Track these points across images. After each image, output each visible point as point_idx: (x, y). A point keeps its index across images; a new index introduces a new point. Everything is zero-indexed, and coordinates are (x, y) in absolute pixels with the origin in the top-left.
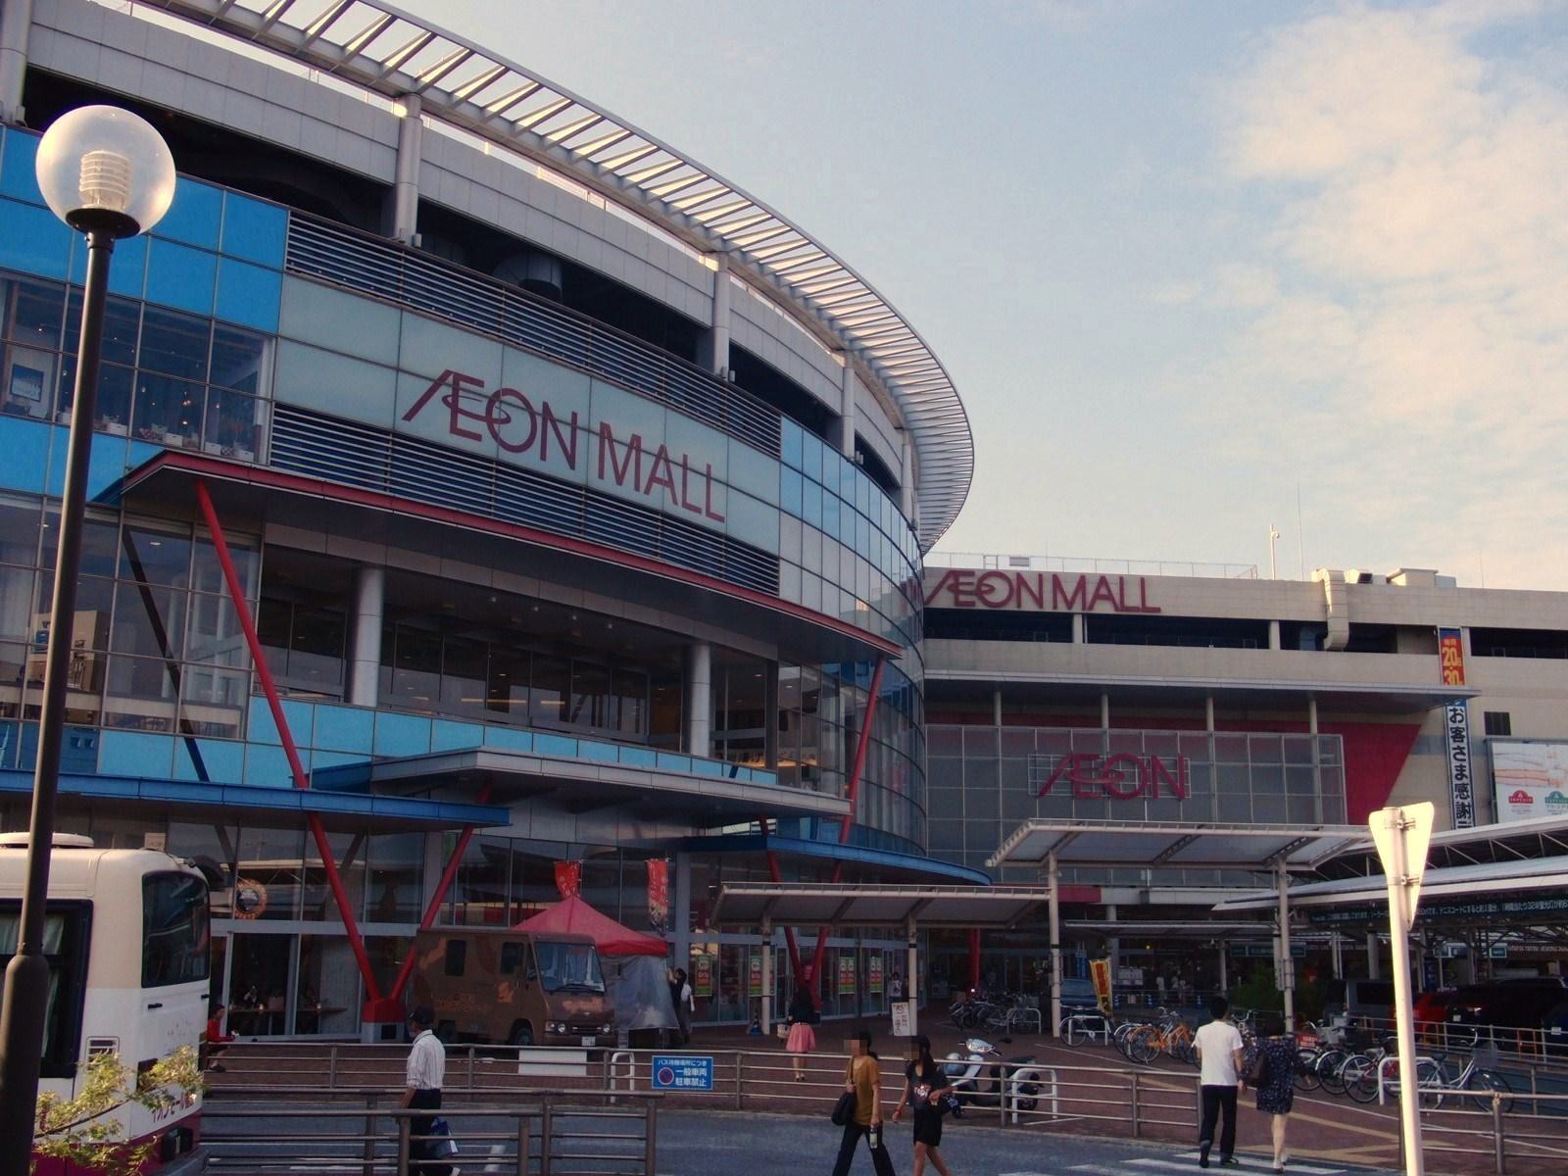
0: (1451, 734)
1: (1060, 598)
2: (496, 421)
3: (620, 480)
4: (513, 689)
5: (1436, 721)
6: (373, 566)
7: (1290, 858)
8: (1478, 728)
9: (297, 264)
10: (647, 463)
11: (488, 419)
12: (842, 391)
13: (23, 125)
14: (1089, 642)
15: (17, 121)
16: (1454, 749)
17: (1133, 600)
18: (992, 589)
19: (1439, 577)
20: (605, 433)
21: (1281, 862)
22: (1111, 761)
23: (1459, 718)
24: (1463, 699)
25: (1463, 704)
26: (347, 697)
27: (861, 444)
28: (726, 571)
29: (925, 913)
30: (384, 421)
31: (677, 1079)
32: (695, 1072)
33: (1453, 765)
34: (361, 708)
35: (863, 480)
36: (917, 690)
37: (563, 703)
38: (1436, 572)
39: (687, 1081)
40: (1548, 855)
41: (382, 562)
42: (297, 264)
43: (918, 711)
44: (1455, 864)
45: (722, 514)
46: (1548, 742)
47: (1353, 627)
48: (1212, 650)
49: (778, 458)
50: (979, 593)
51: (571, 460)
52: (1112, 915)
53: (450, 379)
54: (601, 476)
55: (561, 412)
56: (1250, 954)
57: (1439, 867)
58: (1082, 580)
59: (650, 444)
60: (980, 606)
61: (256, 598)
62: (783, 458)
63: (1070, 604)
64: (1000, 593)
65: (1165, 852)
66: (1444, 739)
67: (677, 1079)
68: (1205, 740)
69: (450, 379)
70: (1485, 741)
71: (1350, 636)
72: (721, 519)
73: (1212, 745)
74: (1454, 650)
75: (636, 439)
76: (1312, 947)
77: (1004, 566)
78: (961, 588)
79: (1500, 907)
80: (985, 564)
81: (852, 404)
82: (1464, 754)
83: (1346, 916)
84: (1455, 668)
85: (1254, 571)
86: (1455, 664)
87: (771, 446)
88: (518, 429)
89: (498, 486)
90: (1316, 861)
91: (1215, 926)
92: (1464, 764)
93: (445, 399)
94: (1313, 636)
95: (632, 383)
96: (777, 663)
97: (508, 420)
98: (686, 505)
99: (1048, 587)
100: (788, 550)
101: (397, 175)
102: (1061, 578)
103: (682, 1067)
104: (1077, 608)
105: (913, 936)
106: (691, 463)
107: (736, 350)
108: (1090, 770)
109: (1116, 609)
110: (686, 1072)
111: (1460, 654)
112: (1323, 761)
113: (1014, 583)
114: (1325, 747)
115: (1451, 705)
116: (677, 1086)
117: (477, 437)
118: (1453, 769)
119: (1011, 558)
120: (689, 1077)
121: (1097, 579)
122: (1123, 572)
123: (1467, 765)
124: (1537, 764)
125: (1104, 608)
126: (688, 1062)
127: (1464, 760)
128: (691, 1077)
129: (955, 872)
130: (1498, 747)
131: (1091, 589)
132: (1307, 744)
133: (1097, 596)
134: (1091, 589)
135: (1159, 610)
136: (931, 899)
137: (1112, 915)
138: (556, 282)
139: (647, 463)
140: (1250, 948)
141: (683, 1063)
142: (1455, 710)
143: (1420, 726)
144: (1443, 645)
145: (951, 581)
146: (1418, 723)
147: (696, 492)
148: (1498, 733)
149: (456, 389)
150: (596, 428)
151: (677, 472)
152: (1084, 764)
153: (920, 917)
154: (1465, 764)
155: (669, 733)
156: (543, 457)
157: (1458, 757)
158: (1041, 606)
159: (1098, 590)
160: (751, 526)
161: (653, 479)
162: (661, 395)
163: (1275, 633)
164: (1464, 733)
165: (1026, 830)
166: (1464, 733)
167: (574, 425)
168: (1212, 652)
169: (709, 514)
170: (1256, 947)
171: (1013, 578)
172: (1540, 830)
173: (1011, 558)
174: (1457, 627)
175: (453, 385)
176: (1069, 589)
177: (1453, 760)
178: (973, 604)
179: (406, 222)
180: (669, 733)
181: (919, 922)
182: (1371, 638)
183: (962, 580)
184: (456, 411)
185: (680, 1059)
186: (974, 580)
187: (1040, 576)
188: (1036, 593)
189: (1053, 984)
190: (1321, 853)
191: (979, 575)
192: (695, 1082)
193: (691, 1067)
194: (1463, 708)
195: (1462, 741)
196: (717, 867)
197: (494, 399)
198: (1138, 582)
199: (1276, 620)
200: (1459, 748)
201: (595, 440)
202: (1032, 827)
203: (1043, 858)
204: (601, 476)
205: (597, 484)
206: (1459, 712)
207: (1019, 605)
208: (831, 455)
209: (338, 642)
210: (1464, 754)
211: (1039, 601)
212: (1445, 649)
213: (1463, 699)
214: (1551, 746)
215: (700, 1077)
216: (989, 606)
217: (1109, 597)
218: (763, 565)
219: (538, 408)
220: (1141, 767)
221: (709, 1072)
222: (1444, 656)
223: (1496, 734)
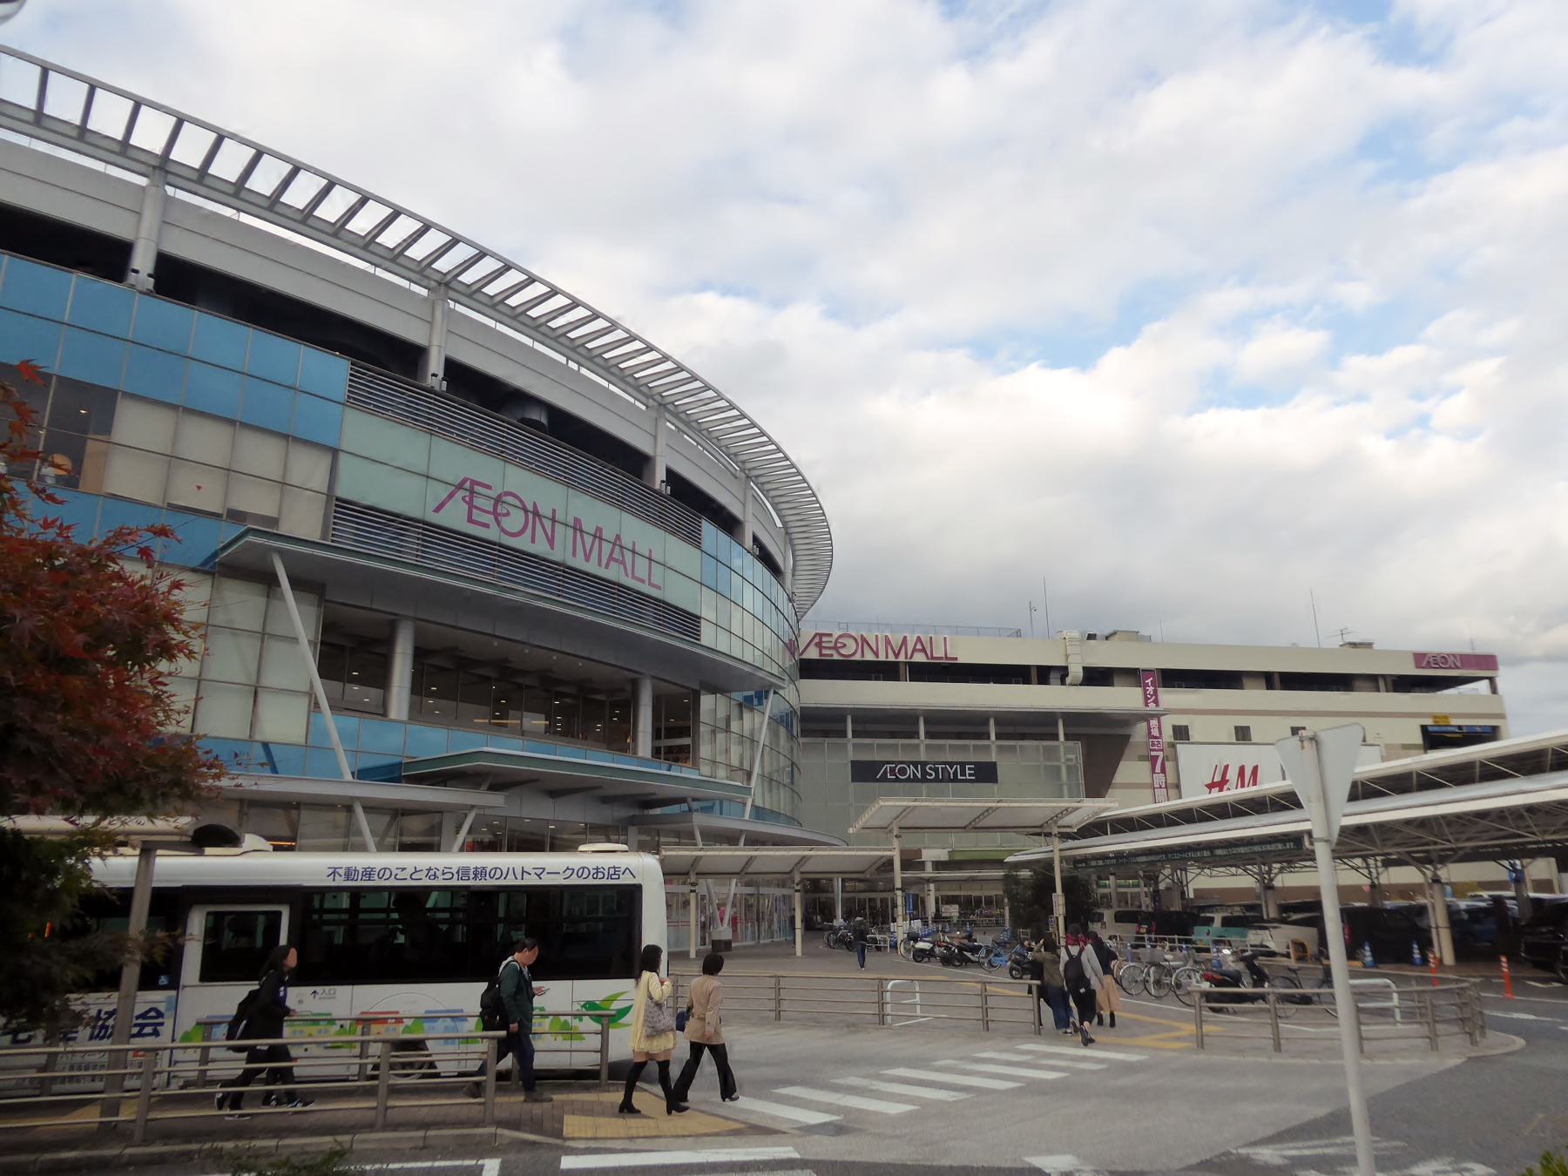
2: (500, 514)
3: (587, 558)
4: (511, 712)
6: (406, 618)
7: (1061, 823)
9: (354, 399)
10: (607, 548)
11: (496, 515)
12: (744, 505)
13: (152, 292)
15: (148, 290)
19: (1141, 636)
20: (577, 527)
21: (1053, 825)
23: (600, 875)
24: (1158, 716)
26: (384, 714)
27: (756, 540)
28: (663, 621)
29: (807, 867)
30: (415, 512)
34: (395, 721)
35: (759, 566)
36: (796, 713)
37: (548, 722)
40: (1234, 816)
41: (412, 614)
42: (354, 399)
43: (796, 728)
44: (1235, 815)
48: (992, 685)
49: (699, 547)
50: (835, 648)
51: (551, 541)
52: (929, 867)
53: (467, 485)
54: (574, 554)
55: (545, 510)
57: (1131, 831)
59: (609, 534)
60: (836, 657)
61: (318, 639)
63: (897, 656)
65: (974, 820)
69: (467, 485)
72: (659, 588)
75: (599, 530)
78: (824, 645)
79: (1212, 852)
81: (751, 515)
83: (1101, 863)
87: (694, 539)
88: (515, 521)
89: (500, 556)
90: (1076, 825)
93: (463, 498)
94: (1059, 676)
95: (598, 493)
97: (508, 514)
98: (634, 577)
100: (707, 612)
101: (430, 341)
106: (637, 549)
107: (670, 472)
109: (928, 658)
114: (1068, 750)
117: (486, 526)
125: (919, 658)
129: (816, 837)
133: (915, 650)
135: (956, 659)
136: (811, 856)
137: (929, 867)
138: (544, 420)
139: (607, 548)
145: (817, 640)
149: (472, 492)
150: (571, 522)
151: (628, 556)
153: (802, 869)
155: (620, 739)
156: (533, 541)
158: (877, 656)
159: (915, 645)
160: (679, 594)
161: (611, 558)
162: (620, 503)
163: (1034, 674)
165: (877, 806)
167: (554, 520)
169: (650, 584)
172: (1194, 805)
175: (468, 488)
178: (832, 655)
179: (435, 365)
180: (620, 739)
181: (802, 873)
182: (1097, 677)
183: (824, 639)
184: (471, 506)
190: (1080, 819)
196: (657, 839)
197: (498, 500)
201: (570, 532)
202: (882, 803)
203: (889, 825)
204: (574, 554)
205: (571, 562)
207: (863, 655)
208: (736, 548)
209: (379, 677)
211: (876, 654)
213: (1158, 716)
217: (924, 650)
218: (689, 622)
219: (530, 507)
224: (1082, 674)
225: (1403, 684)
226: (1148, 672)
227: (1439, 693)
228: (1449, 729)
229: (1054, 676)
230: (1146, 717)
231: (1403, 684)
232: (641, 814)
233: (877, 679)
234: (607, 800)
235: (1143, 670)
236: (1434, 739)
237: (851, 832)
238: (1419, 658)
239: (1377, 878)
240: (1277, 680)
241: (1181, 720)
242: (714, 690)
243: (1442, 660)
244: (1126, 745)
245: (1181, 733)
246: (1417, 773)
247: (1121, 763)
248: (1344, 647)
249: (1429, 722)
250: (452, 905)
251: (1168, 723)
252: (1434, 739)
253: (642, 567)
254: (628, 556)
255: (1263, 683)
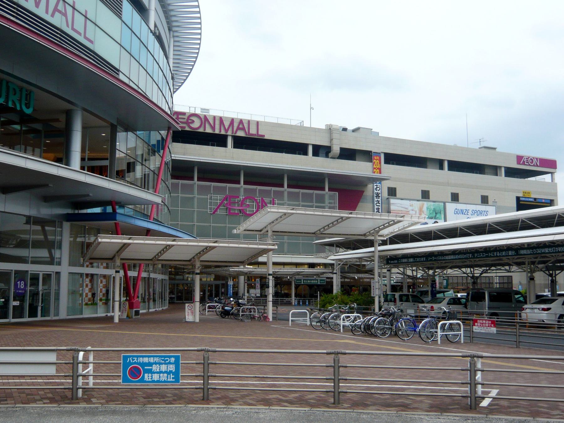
0: (375, 195)
1: (222, 128)
5: (370, 189)
8: (385, 194)
14: (234, 148)
16: (376, 201)
17: (253, 131)
18: (193, 122)
22: (244, 200)
23: (378, 189)
25: (380, 183)
31: (146, 375)
32: (164, 368)
33: (375, 208)
38: (372, 129)
39: (156, 377)
45: (92, 39)
46: (410, 200)
47: (342, 149)
48: (284, 154)
49: (120, 18)
56: (303, 282)
58: (232, 121)
60: (187, 129)
62: (123, 19)
63: (227, 131)
64: (196, 124)
66: (373, 196)
67: (146, 375)
68: (283, 192)
70: (388, 198)
71: (340, 153)
73: (286, 194)
74: (378, 161)
76: (328, 280)
77: (198, 112)
80: (190, 110)
82: (379, 204)
84: (378, 169)
85: (302, 123)
86: (378, 167)
91: (310, 271)
92: (379, 207)
96: (116, 126)
99: (217, 122)
102: (224, 119)
103: (150, 364)
104: (229, 133)
105: (198, 268)
108: (235, 203)
109: (246, 134)
110: (155, 368)
111: (380, 163)
112: (329, 203)
113: (203, 120)
114: (331, 197)
115: (375, 183)
116: (146, 382)
118: (375, 209)
119: (201, 109)
120: (157, 373)
121: (239, 121)
122: (249, 118)
123: (380, 208)
124: (406, 208)
125: (241, 134)
126: (157, 359)
127: (379, 206)
128: (160, 372)
130: (392, 201)
131: (236, 125)
132: (323, 196)
133: (238, 128)
134: (236, 125)
140: (304, 280)
141: (152, 360)
142: (377, 185)
143: (364, 191)
144: (374, 159)
146: (363, 190)
147: (79, 20)
148: (392, 196)
152: (232, 200)
154: (380, 207)
157: (377, 204)
164: (380, 195)
166: (380, 195)
168: (284, 155)
169: (86, 38)
170: (306, 280)
171: (202, 117)
173: (201, 109)
174: (379, 152)
176: (227, 124)
177: (375, 206)
178: (185, 127)
183: (180, 116)
185: (149, 357)
186: (186, 117)
187: (214, 117)
188: (213, 125)
189: (269, 294)
191: (187, 115)
192: (164, 377)
193: (160, 364)
194: (380, 185)
195: (379, 198)
198: (256, 123)
199: (311, 144)
200: (378, 201)
202: (269, 210)
206: (378, 186)
207: (205, 129)
210: (379, 204)
211: (213, 128)
212: (375, 161)
214: (411, 201)
215: (169, 373)
216: (192, 129)
217: (243, 129)
220: (258, 203)
221: (177, 368)
222: (374, 163)
223: (391, 196)
224: (339, 151)
225: (511, 173)
226: (378, 154)
227: (526, 179)
228: (530, 200)
229: (321, 152)
230: (374, 180)
231: (511, 173)
232: (73, 212)
233: (300, 154)
234: (47, 199)
235: (374, 153)
236: (521, 205)
237: (235, 232)
238: (519, 159)
239: (555, 277)
240: (446, 165)
241: (392, 184)
242: (127, 129)
243: (530, 161)
244: (361, 197)
245: (392, 192)
246: (489, 224)
247: (359, 203)
248: (482, 149)
249: (520, 195)
250: (150, 133)
251: (386, 185)
252: (521, 205)
253: (79, 20)
254: (69, 10)
255: (438, 166)
